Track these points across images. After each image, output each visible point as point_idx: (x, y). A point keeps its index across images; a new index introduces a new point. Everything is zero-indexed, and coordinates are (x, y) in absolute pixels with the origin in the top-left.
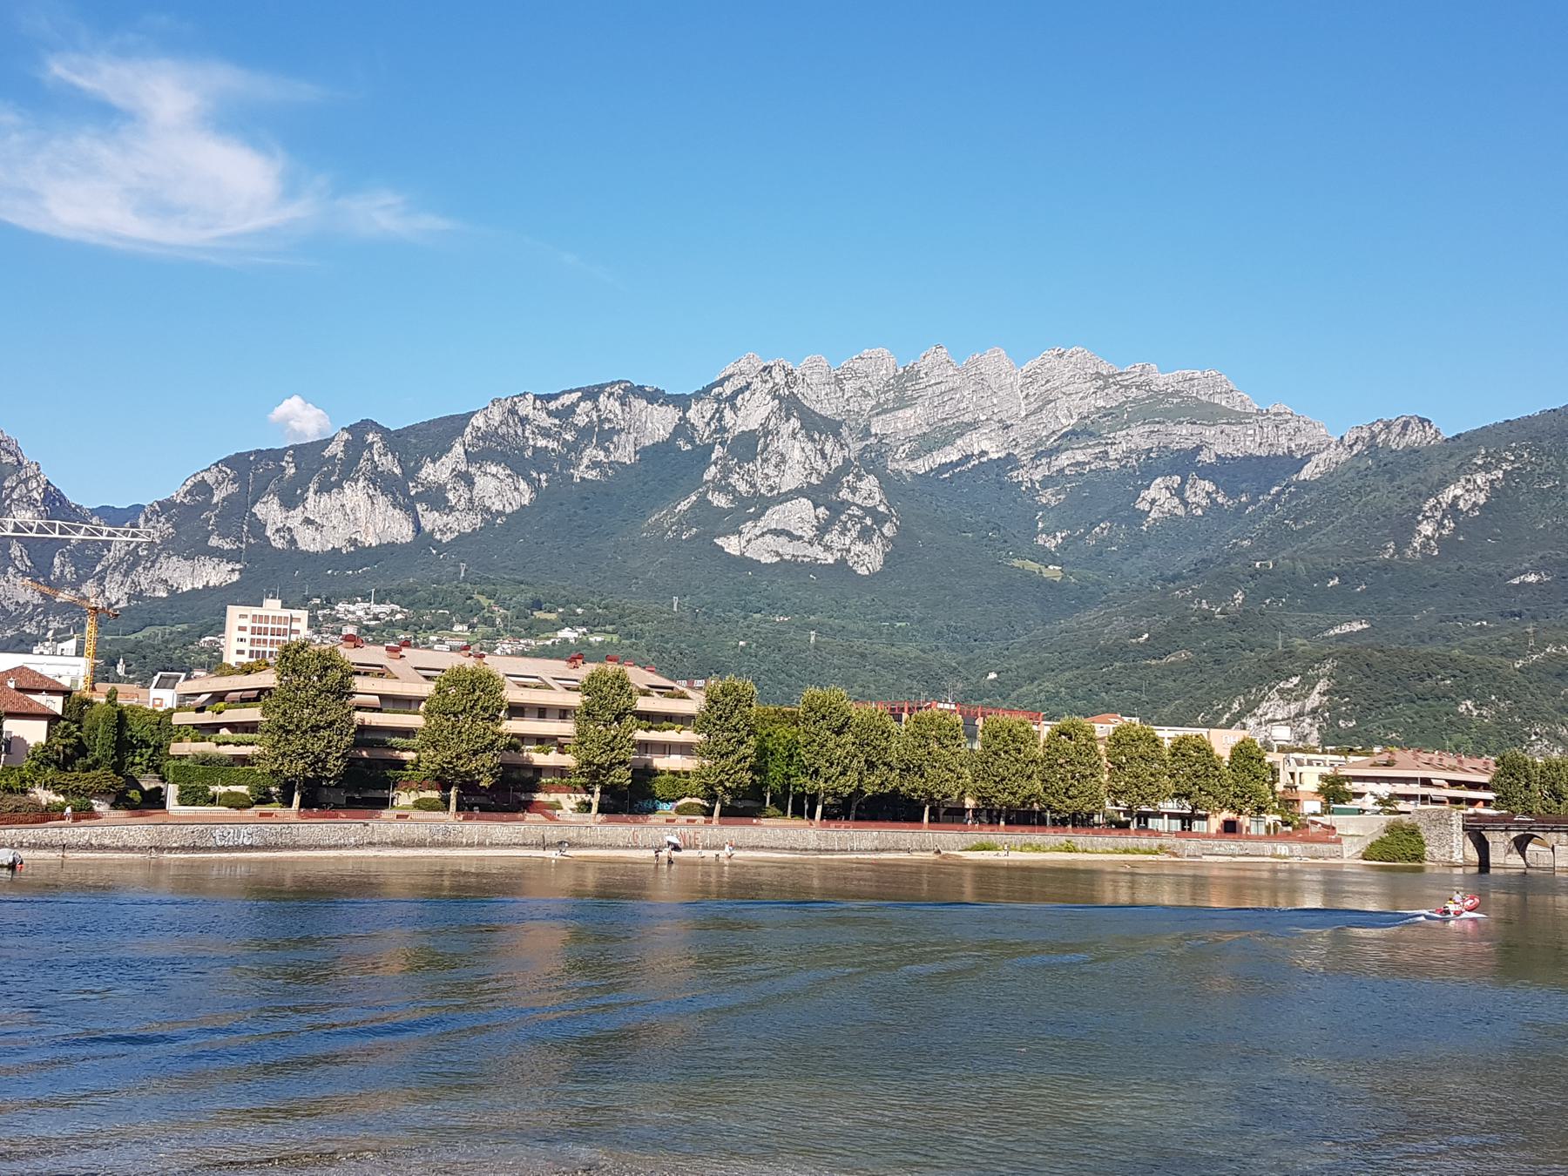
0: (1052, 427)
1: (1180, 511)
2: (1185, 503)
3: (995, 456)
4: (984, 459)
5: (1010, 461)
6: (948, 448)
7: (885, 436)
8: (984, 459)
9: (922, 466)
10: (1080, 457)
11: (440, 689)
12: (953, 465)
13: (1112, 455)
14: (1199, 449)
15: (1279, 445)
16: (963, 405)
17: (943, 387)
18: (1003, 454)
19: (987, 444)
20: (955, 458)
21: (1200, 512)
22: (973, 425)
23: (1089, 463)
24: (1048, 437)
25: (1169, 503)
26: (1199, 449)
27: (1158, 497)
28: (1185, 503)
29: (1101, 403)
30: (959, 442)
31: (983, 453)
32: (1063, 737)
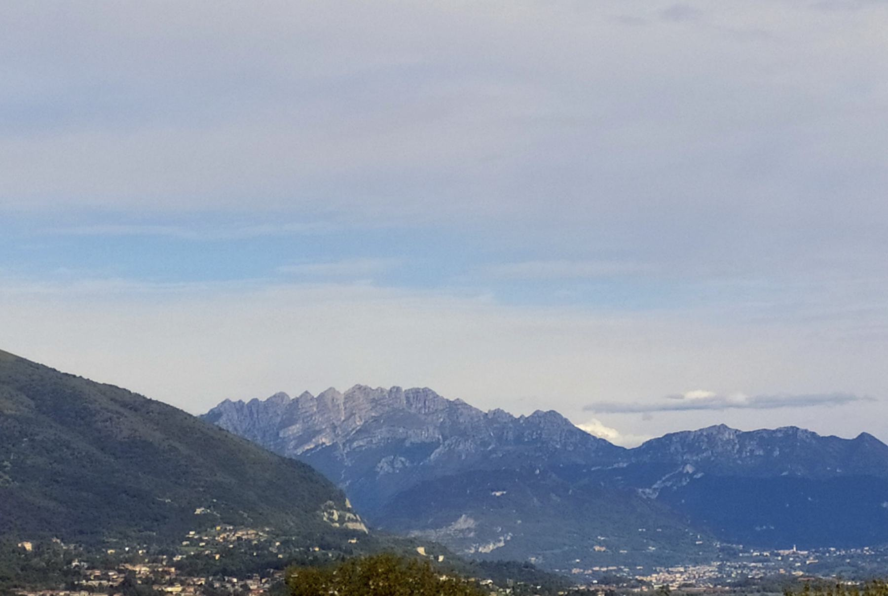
0: (354, 426)
1: (391, 471)
2: (393, 468)
3: (328, 444)
4: (324, 446)
5: (334, 446)
6: (310, 443)
7: (284, 438)
8: (324, 446)
9: (299, 451)
10: (361, 443)
11: (277, 405)
12: (312, 449)
13: (374, 442)
14: (405, 439)
15: (435, 437)
16: (315, 422)
17: (308, 414)
18: (331, 444)
19: (325, 440)
20: (312, 446)
21: (398, 471)
22: (319, 432)
23: (364, 446)
24: (351, 431)
25: (386, 468)
26: (405, 439)
27: (383, 466)
28: (393, 468)
29: (373, 414)
30: (314, 440)
31: (323, 443)
32: (719, 586)
